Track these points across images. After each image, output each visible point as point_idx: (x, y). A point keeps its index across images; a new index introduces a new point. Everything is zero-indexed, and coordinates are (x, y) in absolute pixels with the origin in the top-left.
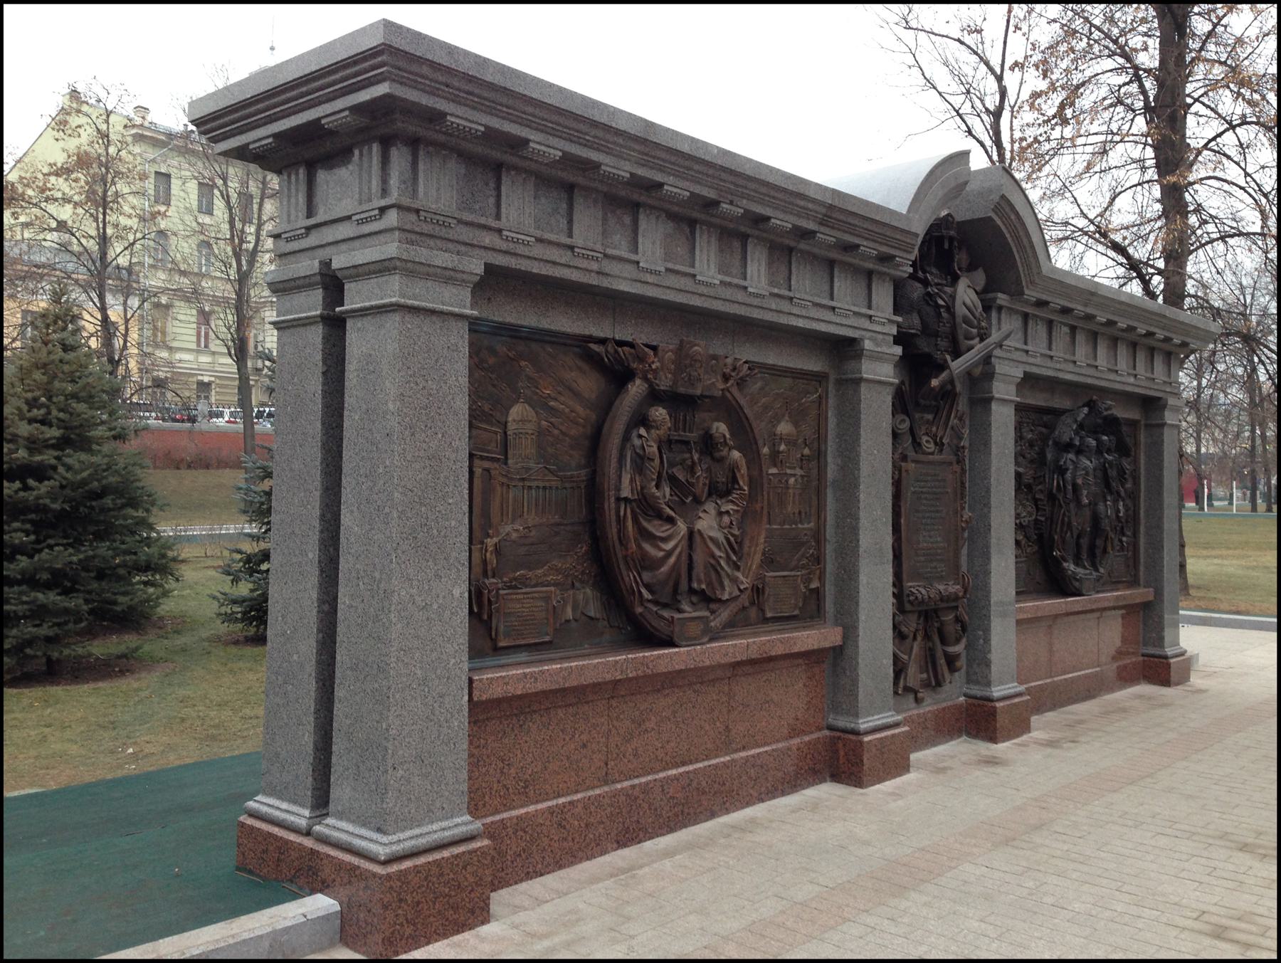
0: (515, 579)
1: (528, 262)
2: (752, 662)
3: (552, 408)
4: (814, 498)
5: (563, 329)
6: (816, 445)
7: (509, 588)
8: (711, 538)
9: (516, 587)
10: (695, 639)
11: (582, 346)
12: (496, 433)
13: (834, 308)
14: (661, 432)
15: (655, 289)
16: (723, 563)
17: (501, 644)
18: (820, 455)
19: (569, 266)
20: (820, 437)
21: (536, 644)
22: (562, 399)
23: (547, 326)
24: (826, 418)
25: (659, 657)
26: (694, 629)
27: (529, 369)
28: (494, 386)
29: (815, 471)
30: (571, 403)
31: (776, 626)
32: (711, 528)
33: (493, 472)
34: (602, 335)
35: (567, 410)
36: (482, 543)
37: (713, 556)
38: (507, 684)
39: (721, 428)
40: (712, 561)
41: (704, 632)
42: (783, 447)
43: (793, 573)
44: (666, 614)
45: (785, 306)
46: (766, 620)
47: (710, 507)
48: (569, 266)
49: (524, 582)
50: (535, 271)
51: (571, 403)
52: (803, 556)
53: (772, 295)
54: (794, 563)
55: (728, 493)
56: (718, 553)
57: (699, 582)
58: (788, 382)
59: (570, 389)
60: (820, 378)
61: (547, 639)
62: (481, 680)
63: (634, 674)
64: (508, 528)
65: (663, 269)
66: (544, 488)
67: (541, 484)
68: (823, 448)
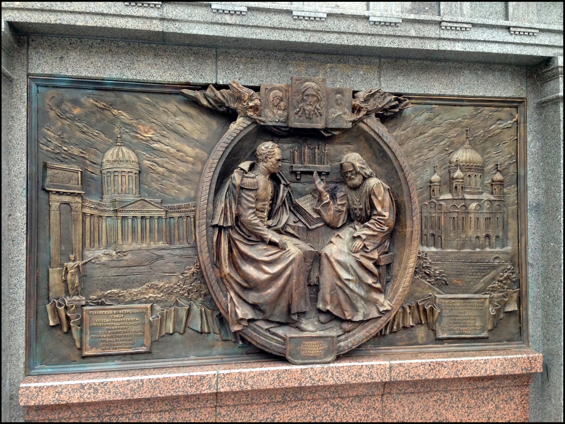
0: (105, 296)
1: (71, 16)
2: (414, 384)
3: (154, 149)
4: (513, 224)
5: (151, 79)
6: (512, 169)
7: (98, 304)
8: (339, 262)
9: (102, 304)
10: (315, 358)
11: (186, 95)
12: (77, 172)
13: (508, 28)
14: (269, 164)
15: (240, 29)
16: (351, 285)
17: (86, 353)
18: (519, 180)
19: (122, 16)
20: (518, 159)
21: (125, 354)
22: (167, 141)
23: (131, 77)
24: (525, 142)
25: (262, 374)
26: (314, 348)
27: (125, 116)
28: (84, 132)
29: (512, 198)
30: (177, 144)
31: (454, 347)
32: (340, 251)
33: (73, 205)
34: (201, 81)
35: (172, 150)
36: (62, 265)
37: (339, 278)
38: (61, 392)
39: (354, 158)
40: (339, 283)
41: (327, 353)
42: (458, 173)
43: (477, 296)
44: (280, 331)
45: (432, 31)
46: (441, 341)
47: (346, 233)
48: (122, 16)
49: (118, 299)
50: (79, 24)
51: (177, 144)
52: (493, 279)
53: (406, 21)
54: (479, 286)
55: (368, 218)
56: (344, 275)
57: (325, 302)
58: (468, 111)
59: (176, 132)
60: (515, 103)
61: (143, 349)
62: (28, 388)
63: (227, 389)
64: (99, 253)
65: (246, 10)
66: (142, 218)
67: (139, 215)
68: (522, 173)
